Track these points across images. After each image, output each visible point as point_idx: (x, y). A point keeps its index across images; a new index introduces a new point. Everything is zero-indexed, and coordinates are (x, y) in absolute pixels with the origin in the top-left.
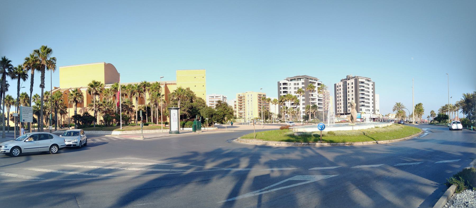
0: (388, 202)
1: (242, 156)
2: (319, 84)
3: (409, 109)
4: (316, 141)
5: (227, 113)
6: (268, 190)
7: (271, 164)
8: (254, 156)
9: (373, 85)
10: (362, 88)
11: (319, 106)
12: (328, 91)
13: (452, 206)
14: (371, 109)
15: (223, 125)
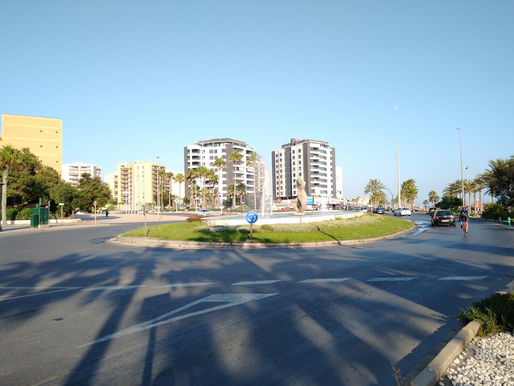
0: (358, 341)
1: (124, 266)
2: (248, 152)
3: (392, 190)
4: (243, 240)
5: (99, 195)
6: (166, 319)
7: (171, 277)
8: (144, 264)
9: (333, 152)
10: (315, 158)
11: (248, 186)
12: (262, 163)
13: (472, 359)
14: (329, 189)
15: (92, 215)
